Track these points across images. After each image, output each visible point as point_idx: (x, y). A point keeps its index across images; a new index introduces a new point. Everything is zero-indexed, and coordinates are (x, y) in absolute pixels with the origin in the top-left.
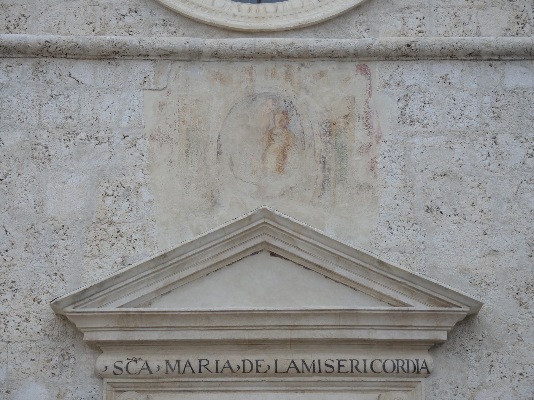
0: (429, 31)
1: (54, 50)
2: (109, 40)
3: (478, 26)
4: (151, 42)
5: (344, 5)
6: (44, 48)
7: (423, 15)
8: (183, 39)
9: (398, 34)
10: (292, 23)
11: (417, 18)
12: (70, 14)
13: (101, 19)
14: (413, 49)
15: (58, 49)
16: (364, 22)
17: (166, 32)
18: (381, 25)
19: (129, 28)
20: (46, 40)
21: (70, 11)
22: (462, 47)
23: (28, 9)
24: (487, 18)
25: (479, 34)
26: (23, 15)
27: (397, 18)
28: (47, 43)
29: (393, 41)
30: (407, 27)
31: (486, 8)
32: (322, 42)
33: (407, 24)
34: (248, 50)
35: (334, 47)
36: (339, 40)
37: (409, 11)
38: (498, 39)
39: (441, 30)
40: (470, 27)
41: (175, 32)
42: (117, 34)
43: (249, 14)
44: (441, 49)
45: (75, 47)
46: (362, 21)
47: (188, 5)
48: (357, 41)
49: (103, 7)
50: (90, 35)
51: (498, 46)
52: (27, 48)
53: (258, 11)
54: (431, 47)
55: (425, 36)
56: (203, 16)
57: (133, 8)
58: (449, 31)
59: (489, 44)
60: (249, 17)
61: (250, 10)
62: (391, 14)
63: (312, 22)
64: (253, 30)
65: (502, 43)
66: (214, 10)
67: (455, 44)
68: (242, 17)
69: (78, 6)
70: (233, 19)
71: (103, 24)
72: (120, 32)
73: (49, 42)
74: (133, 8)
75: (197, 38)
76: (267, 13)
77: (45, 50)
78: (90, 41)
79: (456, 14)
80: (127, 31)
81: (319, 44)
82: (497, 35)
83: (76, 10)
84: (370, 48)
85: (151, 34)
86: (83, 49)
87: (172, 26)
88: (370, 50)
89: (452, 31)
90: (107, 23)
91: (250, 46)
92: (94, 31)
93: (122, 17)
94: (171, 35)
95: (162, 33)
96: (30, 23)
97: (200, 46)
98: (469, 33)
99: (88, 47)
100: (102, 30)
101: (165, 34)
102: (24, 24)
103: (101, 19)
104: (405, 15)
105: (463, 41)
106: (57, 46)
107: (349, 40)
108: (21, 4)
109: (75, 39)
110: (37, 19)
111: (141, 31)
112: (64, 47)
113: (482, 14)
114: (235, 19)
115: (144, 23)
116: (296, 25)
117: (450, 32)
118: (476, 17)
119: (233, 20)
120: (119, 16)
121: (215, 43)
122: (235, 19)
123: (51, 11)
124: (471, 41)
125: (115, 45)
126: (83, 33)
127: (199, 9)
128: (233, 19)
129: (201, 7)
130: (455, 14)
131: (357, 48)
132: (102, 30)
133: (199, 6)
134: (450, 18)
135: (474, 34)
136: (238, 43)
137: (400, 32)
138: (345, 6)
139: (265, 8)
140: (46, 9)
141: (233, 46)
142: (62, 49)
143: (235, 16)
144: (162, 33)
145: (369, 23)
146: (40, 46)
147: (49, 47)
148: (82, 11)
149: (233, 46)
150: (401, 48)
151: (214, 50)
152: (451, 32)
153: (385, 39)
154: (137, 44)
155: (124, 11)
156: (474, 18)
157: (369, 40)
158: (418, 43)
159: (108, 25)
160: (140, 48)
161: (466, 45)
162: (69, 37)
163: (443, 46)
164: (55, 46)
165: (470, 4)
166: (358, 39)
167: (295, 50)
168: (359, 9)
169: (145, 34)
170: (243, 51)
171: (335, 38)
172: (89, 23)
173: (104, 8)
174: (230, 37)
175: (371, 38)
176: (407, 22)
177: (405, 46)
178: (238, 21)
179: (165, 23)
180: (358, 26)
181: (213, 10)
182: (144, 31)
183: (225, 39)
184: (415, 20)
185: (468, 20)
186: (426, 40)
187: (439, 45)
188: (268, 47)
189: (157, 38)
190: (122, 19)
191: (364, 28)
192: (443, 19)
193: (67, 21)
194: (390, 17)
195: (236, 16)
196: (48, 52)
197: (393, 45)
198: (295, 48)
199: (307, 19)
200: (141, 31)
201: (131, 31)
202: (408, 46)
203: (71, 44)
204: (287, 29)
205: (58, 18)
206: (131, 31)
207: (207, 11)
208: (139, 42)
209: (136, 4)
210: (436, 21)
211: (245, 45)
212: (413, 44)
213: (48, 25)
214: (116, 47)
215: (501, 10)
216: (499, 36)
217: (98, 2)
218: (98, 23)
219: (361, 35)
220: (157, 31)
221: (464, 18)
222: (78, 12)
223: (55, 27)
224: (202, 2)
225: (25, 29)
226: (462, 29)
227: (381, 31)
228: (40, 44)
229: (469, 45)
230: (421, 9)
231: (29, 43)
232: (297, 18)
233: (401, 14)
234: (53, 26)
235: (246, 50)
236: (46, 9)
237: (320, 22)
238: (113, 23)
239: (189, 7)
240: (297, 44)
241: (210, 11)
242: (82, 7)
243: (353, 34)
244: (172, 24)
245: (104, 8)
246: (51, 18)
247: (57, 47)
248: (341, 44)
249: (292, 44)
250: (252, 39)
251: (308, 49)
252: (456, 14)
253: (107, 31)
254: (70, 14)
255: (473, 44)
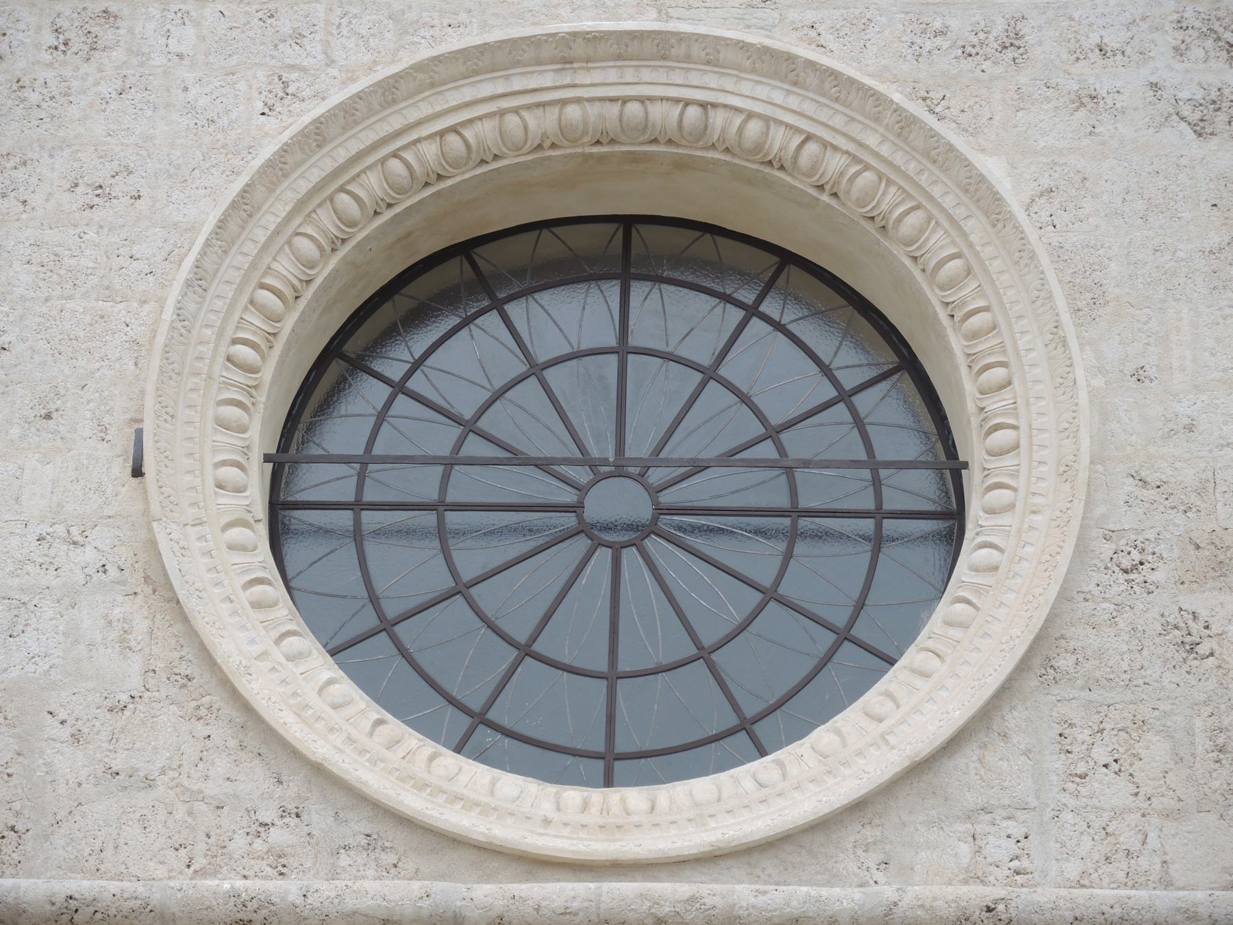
0: (1042, 871)
1: (88, 920)
2: (228, 892)
3: (1165, 862)
4: (333, 894)
5: (824, 799)
6: (62, 914)
7: (1024, 830)
8: (417, 887)
9: (961, 877)
10: (692, 843)
11: (1009, 837)
12: (130, 823)
13: (208, 836)
14: (1000, 920)
15: (99, 916)
16: (875, 843)
17: (373, 865)
18: (917, 853)
19: (280, 857)
20: (69, 893)
21: (131, 816)
22: (1126, 917)
23: (26, 812)
24: (1186, 841)
25: (1167, 884)
26: (13, 829)
27: (959, 835)
28: (71, 901)
29: (951, 898)
30: (985, 858)
31: (1182, 814)
32: (768, 896)
33: (983, 852)
34: (581, 914)
35: (801, 908)
36: (813, 891)
37: (988, 817)
38: (1214, 897)
39: (1072, 869)
40: (1144, 863)
41: (395, 866)
42: (247, 874)
43: (584, 819)
44: (1071, 920)
45: (143, 910)
46: (870, 841)
47: (430, 794)
48: (857, 894)
49: (215, 803)
50: (180, 876)
51: (1215, 916)
52: (20, 915)
53: (605, 810)
54: (1048, 915)
55: (1030, 883)
56: (468, 825)
57: (290, 807)
58: (1091, 871)
59: (1192, 910)
60: (582, 826)
61: (585, 806)
62: (943, 824)
63: (743, 842)
64: (593, 861)
65: (1225, 908)
66: (495, 809)
67: (1106, 909)
68: (566, 825)
69: (151, 804)
70: (542, 831)
71: (214, 849)
72: (256, 869)
73: (75, 899)
74: (291, 807)
75: (452, 884)
76: (628, 815)
77: (65, 918)
78: (179, 896)
79: (1109, 830)
80: (274, 865)
81: (761, 901)
82: (1213, 886)
83: (145, 812)
84: (892, 914)
85: (334, 875)
86: (162, 916)
87: (388, 850)
88: (893, 919)
89: (1100, 872)
90: (223, 844)
91: (586, 904)
92: (189, 866)
93: (261, 829)
94: (385, 874)
95: (362, 868)
96: (29, 848)
97: (459, 904)
98: (1143, 878)
99: (175, 909)
100: (210, 864)
101: (371, 873)
102: (14, 852)
103: (208, 836)
104: (979, 828)
105: (1127, 900)
106: (97, 909)
107: (837, 891)
108: (8, 799)
109: (140, 889)
110: (47, 838)
111: (308, 864)
112: (113, 911)
113: (1173, 832)
114: (548, 832)
115: (317, 844)
116: (702, 849)
117: (1095, 876)
118: (1159, 837)
119: (541, 835)
120: (255, 827)
121: (496, 895)
122: (548, 832)
123: (84, 816)
124: (1148, 902)
125: (244, 905)
126: (161, 872)
127: (458, 806)
128: (542, 831)
129: (462, 799)
130: (1104, 829)
131: (860, 913)
132: (210, 864)
133: (458, 798)
134: (1093, 839)
135: (1154, 882)
136: (554, 897)
137: (967, 870)
138: (826, 802)
139: (623, 801)
140: (71, 812)
141: (544, 904)
142: (108, 916)
143: (547, 822)
144: (362, 868)
145: (887, 847)
146: (54, 908)
147: (76, 911)
148: (162, 815)
149: (544, 904)
150: (971, 916)
151: (493, 914)
152: (1096, 875)
153: (930, 891)
154: (299, 901)
155: (268, 813)
156: (1153, 841)
157: (888, 892)
158: (1014, 905)
159: (225, 851)
160: (307, 912)
161: (1134, 912)
162: (126, 884)
163: (1078, 914)
164: (92, 909)
165: (1141, 805)
166: (862, 889)
167: (702, 916)
168: (861, 811)
169: (318, 873)
170: (568, 917)
171: (800, 883)
172: (177, 846)
173: (218, 807)
174: (536, 880)
175: (895, 887)
176: (983, 846)
177: (982, 910)
178: (556, 836)
179: (371, 843)
180: (860, 852)
181: (493, 809)
182: (317, 865)
183: (524, 886)
184: (1004, 842)
185: (1139, 845)
186: (1034, 895)
187: (1067, 910)
188: (633, 907)
189: (350, 883)
190: (262, 834)
191: (872, 859)
192: (1074, 842)
193: (122, 841)
194: (941, 832)
195: (551, 821)
196: (72, 923)
197: (950, 906)
198: (701, 911)
199: (731, 833)
200: (308, 864)
201: (284, 866)
202: (989, 910)
203: (132, 904)
204: (681, 859)
205: (99, 833)
206: (284, 866)
207: (479, 809)
208: (305, 896)
209: (299, 796)
210: (1058, 845)
211: (572, 902)
212: (1001, 907)
213: (75, 853)
214: (244, 909)
215: (1222, 821)
216: (1218, 889)
217: (202, 792)
218: (201, 846)
219: (869, 876)
220: (350, 865)
221: (1129, 839)
222: (150, 817)
223: (90, 858)
224: (466, 787)
225: (17, 862)
226: (1125, 868)
227: (919, 866)
228: (53, 904)
229: (1142, 912)
230: (1019, 813)
231: (25, 903)
232: (706, 830)
233: (969, 826)
234: (86, 854)
235: (576, 914)
236: (71, 812)
237: (763, 842)
238: (239, 844)
239: (432, 802)
240: (706, 900)
241: (486, 810)
242: (162, 805)
243: (847, 872)
244: (388, 844)
245: (218, 807)
246: (81, 836)
247: (96, 911)
248: (816, 902)
249: (692, 900)
250: (592, 885)
251: (735, 913)
252: (1109, 830)
253: (223, 865)
254: (130, 823)
255: (1152, 910)
